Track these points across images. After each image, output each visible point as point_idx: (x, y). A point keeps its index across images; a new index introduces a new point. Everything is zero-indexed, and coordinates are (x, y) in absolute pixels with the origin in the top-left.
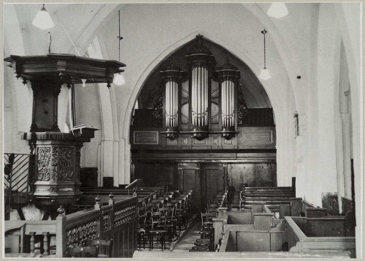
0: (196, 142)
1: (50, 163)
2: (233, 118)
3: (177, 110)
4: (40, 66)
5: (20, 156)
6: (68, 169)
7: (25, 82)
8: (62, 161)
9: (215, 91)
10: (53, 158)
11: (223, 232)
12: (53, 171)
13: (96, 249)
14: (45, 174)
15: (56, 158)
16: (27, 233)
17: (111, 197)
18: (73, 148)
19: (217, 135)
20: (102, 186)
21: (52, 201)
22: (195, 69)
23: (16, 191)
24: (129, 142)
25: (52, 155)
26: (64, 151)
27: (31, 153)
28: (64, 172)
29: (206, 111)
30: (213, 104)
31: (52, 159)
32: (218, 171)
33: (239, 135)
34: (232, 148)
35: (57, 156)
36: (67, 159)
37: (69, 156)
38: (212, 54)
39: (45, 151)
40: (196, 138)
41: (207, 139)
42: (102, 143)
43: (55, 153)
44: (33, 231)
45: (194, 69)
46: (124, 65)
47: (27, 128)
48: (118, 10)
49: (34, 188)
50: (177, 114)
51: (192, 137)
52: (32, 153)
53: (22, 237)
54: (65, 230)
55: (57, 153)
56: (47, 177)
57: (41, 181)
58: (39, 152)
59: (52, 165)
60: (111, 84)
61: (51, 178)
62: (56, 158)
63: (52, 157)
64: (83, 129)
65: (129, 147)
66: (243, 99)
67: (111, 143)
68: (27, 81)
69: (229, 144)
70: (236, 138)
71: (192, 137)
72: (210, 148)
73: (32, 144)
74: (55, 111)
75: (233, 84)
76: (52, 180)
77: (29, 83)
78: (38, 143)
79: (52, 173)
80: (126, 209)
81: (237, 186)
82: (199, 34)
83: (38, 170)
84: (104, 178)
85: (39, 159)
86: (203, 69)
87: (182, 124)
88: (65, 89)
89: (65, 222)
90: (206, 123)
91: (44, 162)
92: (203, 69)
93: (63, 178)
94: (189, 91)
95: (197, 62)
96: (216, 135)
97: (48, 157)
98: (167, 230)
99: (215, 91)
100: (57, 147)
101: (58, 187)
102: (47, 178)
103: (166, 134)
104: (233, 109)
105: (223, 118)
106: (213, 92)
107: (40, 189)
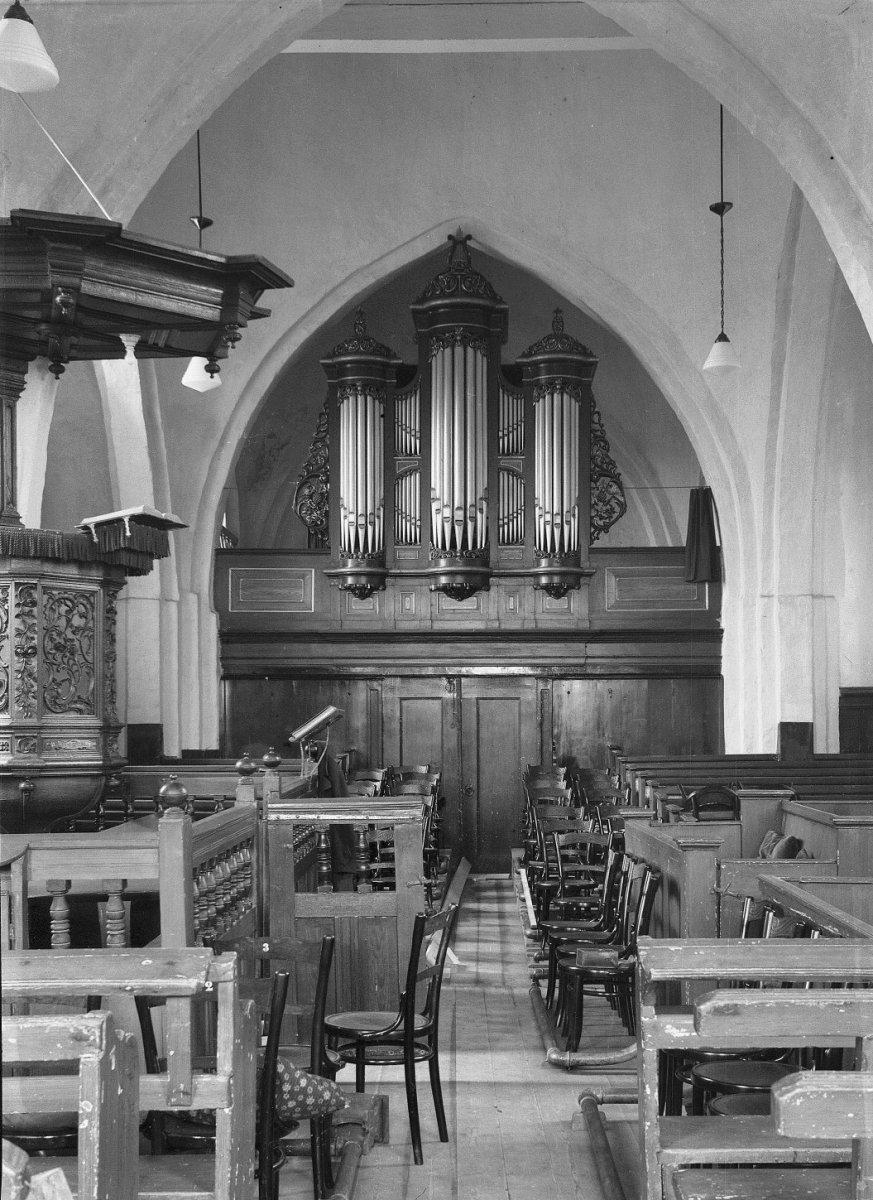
0: (449, 603)
2: (574, 523)
6: (75, 668)
8: (52, 639)
9: (511, 429)
10: (22, 627)
11: (719, 886)
12: (20, 676)
15: (31, 628)
16: (38, 889)
17: (270, 765)
18: (93, 593)
19: (521, 580)
21: (22, 785)
22: (443, 352)
25: (17, 616)
26: (60, 601)
28: (63, 681)
29: (481, 499)
30: (504, 478)
31: (17, 630)
32: (520, 704)
33: (595, 579)
34: (571, 626)
35: (35, 621)
36: (73, 632)
37: (77, 621)
38: (501, 301)
40: (448, 590)
41: (484, 593)
43: (27, 609)
45: (440, 353)
46: (282, 282)
50: (379, 509)
51: (433, 587)
53: (18, 899)
54: (196, 871)
55: (35, 609)
59: (17, 654)
60: (219, 363)
65: (212, 623)
66: (608, 456)
67: (155, 605)
69: (562, 613)
70: (584, 591)
71: (433, 587)
72: (496, 625)
75: (576, 406)
76: (16, 708)
79: (19, 682)
81: (587, 754)
82: (460, 231)
86: (470, 351)
87: (397, 544)
89: (192, 842)
90: (481, 542)
92: (470, 351)
95: (451, 330)
96: (513, 581)
99: (511, 429)
100: (34, 587)
103: (344, 576)
104: (575, 494)
105: (540, 523)
106: (506, 432)
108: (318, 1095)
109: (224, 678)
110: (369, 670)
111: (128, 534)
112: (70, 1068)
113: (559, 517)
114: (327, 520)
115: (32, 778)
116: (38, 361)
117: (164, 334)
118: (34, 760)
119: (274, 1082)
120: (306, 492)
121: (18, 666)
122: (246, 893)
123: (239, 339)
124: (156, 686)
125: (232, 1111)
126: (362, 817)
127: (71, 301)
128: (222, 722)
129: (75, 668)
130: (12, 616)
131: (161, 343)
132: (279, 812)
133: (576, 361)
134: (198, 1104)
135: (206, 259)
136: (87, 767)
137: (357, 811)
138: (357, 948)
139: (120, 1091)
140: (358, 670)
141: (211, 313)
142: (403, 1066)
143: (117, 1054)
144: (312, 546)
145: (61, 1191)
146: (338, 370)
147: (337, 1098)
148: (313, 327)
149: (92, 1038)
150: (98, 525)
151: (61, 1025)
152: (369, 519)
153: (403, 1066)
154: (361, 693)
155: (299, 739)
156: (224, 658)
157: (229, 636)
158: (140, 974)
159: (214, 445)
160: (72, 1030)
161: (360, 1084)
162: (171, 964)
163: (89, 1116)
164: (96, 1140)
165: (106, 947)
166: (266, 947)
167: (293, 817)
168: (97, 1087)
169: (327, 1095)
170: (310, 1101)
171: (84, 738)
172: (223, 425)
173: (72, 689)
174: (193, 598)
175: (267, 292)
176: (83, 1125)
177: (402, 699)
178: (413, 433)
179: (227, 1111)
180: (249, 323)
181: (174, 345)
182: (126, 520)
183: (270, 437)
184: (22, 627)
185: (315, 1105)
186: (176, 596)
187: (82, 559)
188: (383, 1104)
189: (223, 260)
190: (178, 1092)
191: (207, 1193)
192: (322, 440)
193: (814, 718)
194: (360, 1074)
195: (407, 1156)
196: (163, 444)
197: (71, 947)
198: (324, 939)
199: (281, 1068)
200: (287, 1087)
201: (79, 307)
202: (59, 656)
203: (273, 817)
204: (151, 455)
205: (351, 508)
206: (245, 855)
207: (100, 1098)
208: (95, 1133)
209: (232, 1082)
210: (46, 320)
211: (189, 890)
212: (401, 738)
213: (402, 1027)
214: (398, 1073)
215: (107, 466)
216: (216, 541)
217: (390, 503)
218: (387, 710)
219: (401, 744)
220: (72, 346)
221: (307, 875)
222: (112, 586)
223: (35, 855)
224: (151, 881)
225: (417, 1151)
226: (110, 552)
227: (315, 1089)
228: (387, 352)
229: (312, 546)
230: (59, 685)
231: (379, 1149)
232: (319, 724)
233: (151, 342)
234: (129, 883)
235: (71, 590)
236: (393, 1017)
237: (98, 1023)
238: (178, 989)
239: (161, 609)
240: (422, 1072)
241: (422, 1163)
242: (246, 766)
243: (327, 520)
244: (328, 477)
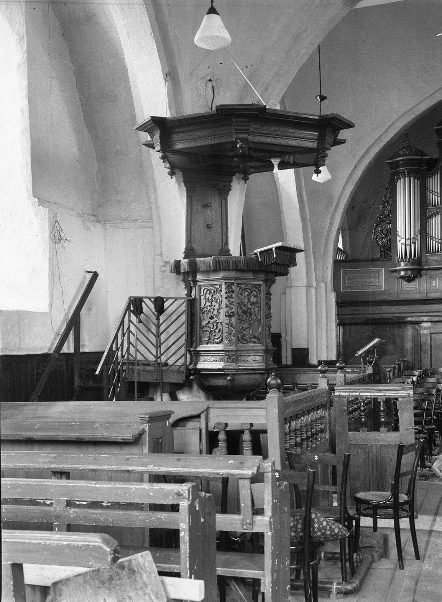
1: (223, 312)
3: (419, 229)
4: (201, 134)
5: (170, 301)
7: (172, 174)
8: (241, 308)
10: (228, 303)
13: (345, 458)
14: (215, 332)
15: (231, 303)
18: (260, 285)
20: (289, 363)
21: (229, 378)
23: (166, 364)
24: (333, 289)
25: (226, 298)
26: (245, 290)
27: (189, 294)
28: (247, 328)
35: (234, 300)
36: (251, 305)
37: (253, 299)
39: (212, 292)
42: (288, 290)
43: (230, 294)
44: (223, 420)
46: (349, 125)
47: (178, 252)
48: (316, 46)
49: (195, 355)
52: (191, 296)
53: (204, 431)
54: (285, 420)
55: (233, 294)
56: (217, 337)
57: (207, 343)
58: (202, 293)
61: (224, 338)
62: (231, 303)
63: (225, 302)
64: (277, 248)
67: (304, 289)
68: (175, 170)
73: (190, 279)
74: (224, 223)
76: (226, 341)
77: (180, 174)
78: (199, 277)
79: (227, 329)
80: (72, 485)
83: (201, 324)
84: (293, 350)
85: (202, 306)
87: (428, 253)
88: (239, 184)
89: (283, 407)
91: (212, 311)
93: (244, 338)
94: (440, 193)
97: (218, 301)
98: (426, 433)
100: (233, 284)
101: (237, 355)
102: (217, 339)
103: (399, 271)
107: (206, 357)
108: (332, 530)
109: (339, 325)
110: (414, 319)
111: (275, 256)
112: (175, 508)
113: (409, 241)
114: (390, 243)
115: (233, 374)
116: (237, 175)
117: (292, 157)
118: (234, 366)
119: (310, 523)
120: (379, 229)
121: (227, 321)
122: (322, 431)
123: (327, 156)
124: (305, 329)
125: (272, 534)
126: (381, 394)
127: (244, 146)
128: (338, 346)
129: (252, 322)
130: (224, 298)
131: (291, 162)
132: (341, 392)
133: (417, 159)
134: (256, 530)
135: (308, 118)
136: (259, 369)
137: (379, 391)
138: (380, 459)
139: (202, 520)
140: (409, 319)
141: (313, 145)
142: (393, 520)
143: (199, 503)
144: (383, 257)
145: (148, 561)
146: (396, 165)
147: (342, 532)
148: (382, 145)
149: (184, 495)
150: (261, 253)
151: (171, 488)
152: (412, 241)
153: (393, 520)
154: (409, 331)
155: (360, 355)
156: (339, 315)
157: (341, 303)
158: (227, 467)
159: (332, 208)
160: (176, 491)
161: (375, 527)
162: (242, 463)
163: (184, 530)
164: (188, 541)
165: (243, 454)
166: (316, 458)
167: (347, 394)
168: (187, 518)
169: (336, 531)
170: (328, 533)
171: (257, 355)
172: (337, 198)
173: (251, 332)
174: (323, 285)
175: (342, 131)
176: (182, 534)
177: (431, 333)
178: (436, 194)
179: (269, 534)
180: (331, 148)
181: (297, 161)
182: (274, 249)
183: (364, 202)
184: (228, 303)
185: (331, 535)
186: (314, 284)
187: (254, 269)
188: (386, 539)
189: (317, 118)
190: (247, 523)
191: (261, 572)
192: (387, 202)
193: (308, 345)
194: (375, 522)
195: (396, 566)
196: (307, 209)
197: (229, 454)
198: (345, 454)
199: (313, 516)
200: (316, 525)
201: (250, 149)
202: (244, 316)
203: (337, 394)
204: (301, 215)
205: (403, 236)
206: (321, 412)
207: (189, 523)
208: (187, 538)
209: (272, 520)
210: (237, 156)
211: (281, 428)
212: (431, 354)
213: (392, 500)
214: (390, 523)
215: (281, 222)
216: (335, 256)
217: (424, 232)
218: (423, 340)
219: (431, 356)
220: (251, 167)
221: (355, 426)
222: (269, 282)
223: (211, 411)
224: (263, 424)
225: (400, 563)
226: (267, 265)
227: (331, 526)
228: (423, 154)
229: (383, 257)
230: (245, 330)
231: (383, 560)
232: (369, 348)
233: (286, 161)
234: (228, 425)
235: (249, 284)
236: (388, 494)
237: (187, 488)
238: (244, 475)
239: (307, 291)
240: (404, 523)
241: (403, 569)
242: (323, 369)
243: (390, 243)
244: (390, 220)
